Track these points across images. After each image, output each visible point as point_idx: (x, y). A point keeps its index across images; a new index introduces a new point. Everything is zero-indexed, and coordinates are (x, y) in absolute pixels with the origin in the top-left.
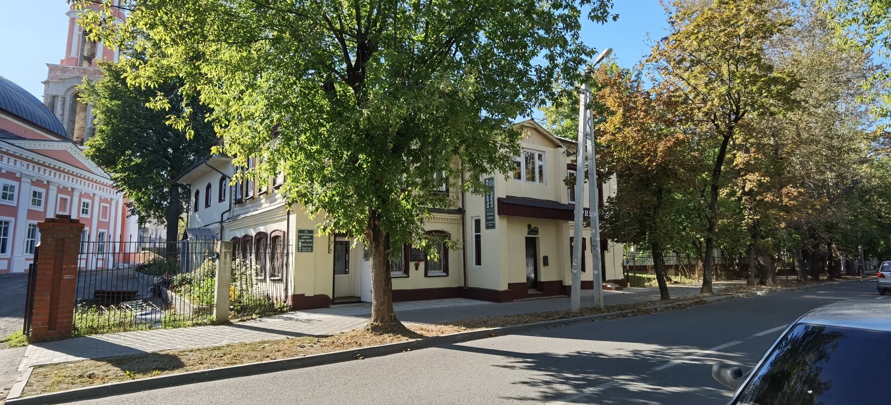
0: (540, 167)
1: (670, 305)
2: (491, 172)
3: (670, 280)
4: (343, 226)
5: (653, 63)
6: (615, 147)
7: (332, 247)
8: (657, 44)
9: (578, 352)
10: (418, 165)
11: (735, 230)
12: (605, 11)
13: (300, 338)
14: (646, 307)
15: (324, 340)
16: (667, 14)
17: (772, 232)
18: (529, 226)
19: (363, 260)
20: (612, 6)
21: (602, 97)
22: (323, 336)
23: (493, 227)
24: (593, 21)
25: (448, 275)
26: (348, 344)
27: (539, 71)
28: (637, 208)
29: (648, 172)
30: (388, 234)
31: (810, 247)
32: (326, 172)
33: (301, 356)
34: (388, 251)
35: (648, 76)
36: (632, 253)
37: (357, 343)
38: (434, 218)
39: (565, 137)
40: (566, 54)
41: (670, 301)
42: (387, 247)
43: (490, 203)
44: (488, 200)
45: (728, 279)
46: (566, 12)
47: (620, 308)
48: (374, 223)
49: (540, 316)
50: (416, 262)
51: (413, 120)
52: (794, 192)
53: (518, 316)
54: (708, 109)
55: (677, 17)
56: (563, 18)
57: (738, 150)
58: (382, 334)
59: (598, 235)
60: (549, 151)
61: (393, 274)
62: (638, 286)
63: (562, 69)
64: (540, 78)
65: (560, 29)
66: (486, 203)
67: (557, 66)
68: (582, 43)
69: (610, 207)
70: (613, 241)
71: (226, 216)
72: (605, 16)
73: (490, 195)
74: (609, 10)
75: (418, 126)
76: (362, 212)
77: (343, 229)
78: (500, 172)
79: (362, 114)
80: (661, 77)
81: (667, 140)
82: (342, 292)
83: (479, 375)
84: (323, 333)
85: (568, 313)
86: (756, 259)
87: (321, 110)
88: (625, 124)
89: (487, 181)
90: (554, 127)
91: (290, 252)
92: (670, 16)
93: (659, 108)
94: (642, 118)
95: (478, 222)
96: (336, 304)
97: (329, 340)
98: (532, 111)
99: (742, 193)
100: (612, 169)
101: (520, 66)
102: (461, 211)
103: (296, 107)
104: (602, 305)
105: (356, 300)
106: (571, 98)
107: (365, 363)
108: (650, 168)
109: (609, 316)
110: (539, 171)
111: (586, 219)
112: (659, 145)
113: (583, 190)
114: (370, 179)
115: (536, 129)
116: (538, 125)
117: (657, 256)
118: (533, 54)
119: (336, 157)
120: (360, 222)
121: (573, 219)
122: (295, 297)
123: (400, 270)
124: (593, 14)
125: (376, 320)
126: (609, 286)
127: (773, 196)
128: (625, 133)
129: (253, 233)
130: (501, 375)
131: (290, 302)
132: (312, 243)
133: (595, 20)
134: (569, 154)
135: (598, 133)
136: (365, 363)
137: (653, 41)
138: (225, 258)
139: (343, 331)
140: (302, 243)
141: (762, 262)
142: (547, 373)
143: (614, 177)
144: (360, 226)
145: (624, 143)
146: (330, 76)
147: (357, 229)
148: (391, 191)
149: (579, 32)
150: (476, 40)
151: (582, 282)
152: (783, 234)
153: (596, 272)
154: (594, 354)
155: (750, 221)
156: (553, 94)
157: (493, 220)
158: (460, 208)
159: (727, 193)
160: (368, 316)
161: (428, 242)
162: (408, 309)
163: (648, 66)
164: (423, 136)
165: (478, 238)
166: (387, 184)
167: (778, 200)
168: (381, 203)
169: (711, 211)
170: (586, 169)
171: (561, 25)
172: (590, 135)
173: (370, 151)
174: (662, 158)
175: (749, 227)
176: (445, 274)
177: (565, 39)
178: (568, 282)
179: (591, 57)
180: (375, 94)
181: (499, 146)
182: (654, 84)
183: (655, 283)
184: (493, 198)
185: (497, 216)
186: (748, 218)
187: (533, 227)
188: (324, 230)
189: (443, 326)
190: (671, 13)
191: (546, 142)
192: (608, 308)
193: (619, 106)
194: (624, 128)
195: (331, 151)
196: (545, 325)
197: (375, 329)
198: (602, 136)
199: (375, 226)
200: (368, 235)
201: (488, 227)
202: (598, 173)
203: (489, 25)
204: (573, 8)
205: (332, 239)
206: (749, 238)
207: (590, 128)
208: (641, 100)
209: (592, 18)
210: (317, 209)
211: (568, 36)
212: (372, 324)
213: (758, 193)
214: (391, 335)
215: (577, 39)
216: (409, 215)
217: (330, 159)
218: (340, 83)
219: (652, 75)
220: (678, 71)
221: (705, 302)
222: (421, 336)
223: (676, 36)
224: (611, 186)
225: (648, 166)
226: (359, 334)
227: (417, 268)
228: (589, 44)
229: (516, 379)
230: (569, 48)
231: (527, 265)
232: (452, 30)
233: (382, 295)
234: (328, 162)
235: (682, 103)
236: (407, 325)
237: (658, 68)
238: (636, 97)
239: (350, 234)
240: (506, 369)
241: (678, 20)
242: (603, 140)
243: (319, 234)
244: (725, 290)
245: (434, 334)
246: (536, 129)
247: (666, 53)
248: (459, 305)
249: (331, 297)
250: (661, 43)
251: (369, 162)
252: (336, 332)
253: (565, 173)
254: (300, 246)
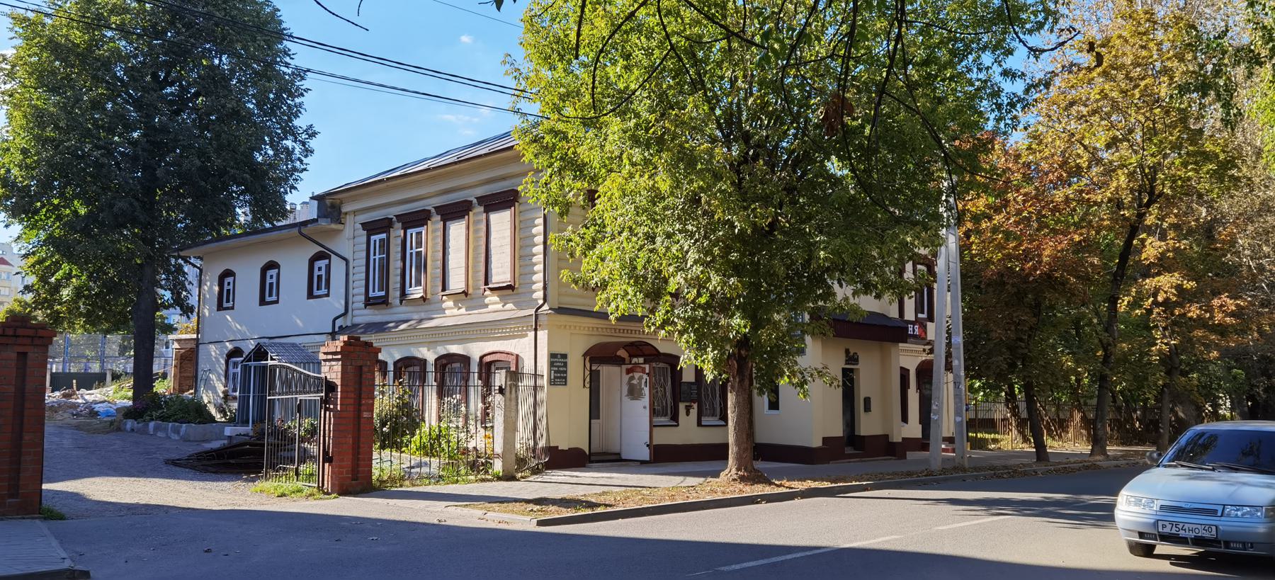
11: (1140, 360)
17: (1200, 364)
18: (847, 351)
19: (626, 400)
31: (1260, 391)
45: (1123, 444)
50: (688, 404)
52: (1231, 305)
54: (1111, 193)
57: (1149, 235)
71: (338, 323)
86: (1172, 410)
96: (592, 462)
99: (1153, 303)
109: (982, 475)
123: (713, 415)
127: (1200, 308)
129: (430, 355)
138: (511, 392)
140: (555, 372)
141: (1181, 414)
152: (1217, 370)
153: (959, 419)
155: (1164, 347)
159: (1129, 302)
167: (1208, 315)
169: (1106, 334)
175: (1163, 356)
176: (723, 423)
186: (1162, 343)
206: (1162, 374)
213: (1177, 304)
221: (1099, 467)
227: (688, 414)
244: (1122, 456)
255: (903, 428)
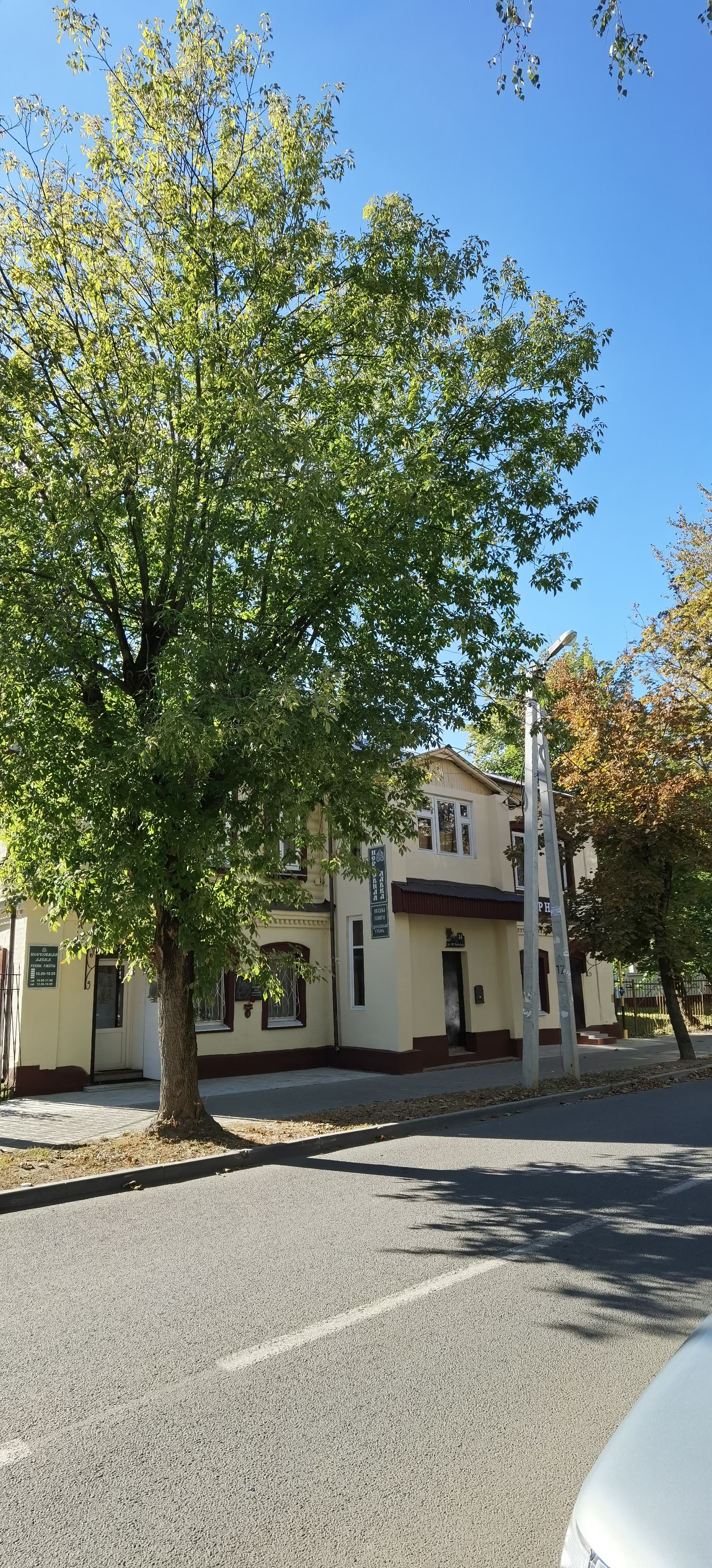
0: (465, 828)
1: (695, 1070)
2: (375, 840)
3: (695, 1022)
4: (109, 942)
5: (648, 653)
6: (590, 793)
7: (91, 978)
8: (651, 622)
9: (532, 1165)
10: (246, 829)
12: (558, 574)
13: (25, 1151)
14: (654, 1074)
15: (70, 1154)
16: (667, 574)
18: (449, 932)
20: (569, 567)
21: (563, 711)
22: (67, 1147)
23: (385, 934)
24: (540, 589)
25: (305, 1026)
26: (114, 1161)
27: (450, 672)
28: (630, 899)
29: (645, 837)
30: (191, 953)
32: (81, 843)
33: (24, 1187)
34: (191, 986)
35: (640, 674)
36: (631, 975)
37: (130, 1159)
38: (275, 920)
39: (506, 775)
40: (495, 643)
41: (696, 1063)
42: (190, 976)
43: (378, 891)
44: (375, 886)
46: (494, 574)
47: (610, 1078)
48: (166, 934)
49: (468, 1098)
50: (246, 1003)
51: (235, 754)
53: (430, 1099)
55: (683, 578)
56: (489, 583)
58: (178, 1142)
59: (566, 947)
60: (478, 799)
61: (200, 1025)
62: (642, 1035)
63: (490, 667)
64: (452, 683)
65: (483, 604)
66: (372, 890)
67: (479, 663)
68: (521, 625)
69: (586, 896)
70: (593, 956)
72: (559, 582)
73: (378, 878)
74: (564, 571)
75: (246, 762)
76: (145, 914)
77: (109, 946)
78: (391, 840)
79: (143, 745)
80: (661, 678)
81: (674, 783)
82: (109, 1060)
83: (353, 1214)
84: (70, 1141)
85: (518, 1092)
87: (75, 735)
88: (603, 755)
89: (373, 853)
90: (489, 757)
91: (15, 986)
92: (672, 577)
93: (663, 729)
94: (632, 746)
95: (358, 926)
96: (97, 1083)
97: (80, 1154)
98: (439, 738)
100: (585, 832)
101: (420, 663)
102: (329, 907)
103: (28, 730)
104: (577, 1074)
105: (135, 1075)
106: (505, 717)
107: (144, 1198)
108: (648, 830)
109: (591, 1093)
110: (463, 835)
111: (544, 916)
112: (661, 791)
113: (536, 867)
114: (161, 853)
115: (455, 764)
116: (459, 756)
117: (668, 983)
118: (442, 643)
119: (100, 815)
120: (140, 933)
121: (522, 919)
122: (21, 1071)
123: (216, 1017)
124: (538, 579)
125: (166, 1116)
126: (591, 1037)
128: (603, 770)
130: (391, 1214)
131: (11, 1081)
132: (55, 970)
133: (543, 588)
134: (512, 806)
135: (558, 772)
136: (144, 1198)
137: (645, 618)
139: (108, 1136)
140: (37, 970)
142: (483, 1207)
143: (589, 844)
144: (141, 940)
145: (602, 786)
146: (92, 677)
147: (134, 946)
148: (199, 876)
149: (516, 609)
150: (347, 620)
151: (540, 1030)
153: (565, 1014)
154: (559, 1166)
156: (475, 710)
157: (385, 921)
158: (326, 901)
160: (154, 1106)
161: (265, 967)
162: (229, 1092)
163: (638, 659)
164: (256, 779)
165: (359, 955)
166: (190, 864)
168: (179, 898)
170: (540, 833)
171: (485, 597)
172: (545, 774)
173: (162, 807)
174: (668, 813)
177: (492, 620)
178: (518, 1033)
179: (536, 649)
180: (271, 597)
181: (387, 795)
182: (650, 688)
183: (669, 1029)
184: (384, 883)
185: (391, 915)
187: (455, 934)
188: (76, 949)
189: (291, 1123)
190: (672, 573)
191: (474, 785)
192: (589, 1079)
193: (591, 725)
194: (602, 762)
195: (90, 807)
196: (477, 1116)
197: (166, 1133)
198: (564, 775)
199: (168, 940)
200: (153, 957)
201: (375, 935)
202: (561, 835)
203: (366, 593)
204: (506, 570)
205: (92, 962)
207: (544, 763)
208: (627, 714)
209: (538, 585)
210: (63, 912)
211: (497, 615)
212: (159, 1123)
214: (195, 1142)
215: (511, 620)
216: (229, 917)
217: (89, 820)
218: (112, 689)
219: (644, 674)
220: (689, 667)
222: (250, 1143)
223: (681, 611)
224: (587, 860)
225: (645, 826)
226: (136, 1140)
227: (248, 1014)
228: (532, 629)
229: (419, 1221)
230: (500, 634)
231: (447, 1002)
232: (306, 603)
233: (179, 1069)
234: (86, 824)
235: (699, 719)
236: (224, 1122)
237: (656, 662)
238: (619, 711)
239: (120, 953)
240: (400, 1201)
241: (684, 583)
242: (567, 782)
243: (67, 958)
245: (275, 1140)
246: (455, 764)
247: (667, 638)
248: (324, 1081)
249: (88, 1070)
250: (659, 620)
251: (159, 824)
252: (94, 1138)
253: (505, 839)
254: (33, 976)
255: (540, 1019)
